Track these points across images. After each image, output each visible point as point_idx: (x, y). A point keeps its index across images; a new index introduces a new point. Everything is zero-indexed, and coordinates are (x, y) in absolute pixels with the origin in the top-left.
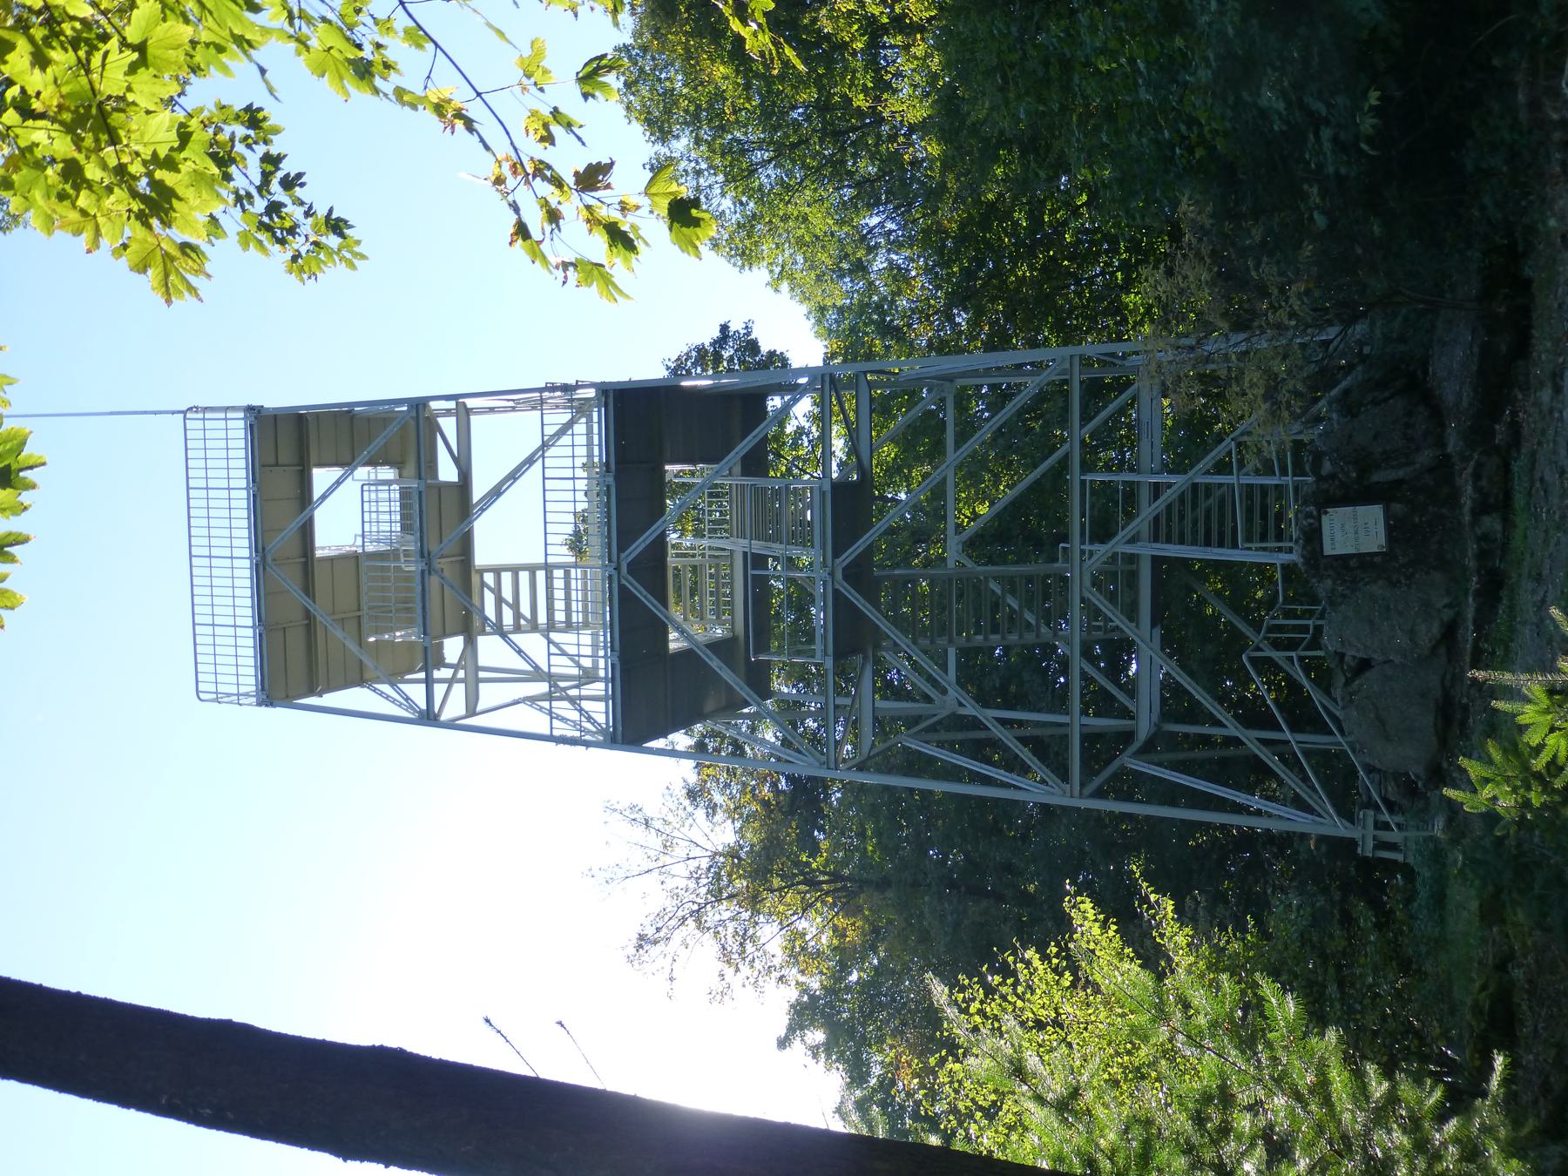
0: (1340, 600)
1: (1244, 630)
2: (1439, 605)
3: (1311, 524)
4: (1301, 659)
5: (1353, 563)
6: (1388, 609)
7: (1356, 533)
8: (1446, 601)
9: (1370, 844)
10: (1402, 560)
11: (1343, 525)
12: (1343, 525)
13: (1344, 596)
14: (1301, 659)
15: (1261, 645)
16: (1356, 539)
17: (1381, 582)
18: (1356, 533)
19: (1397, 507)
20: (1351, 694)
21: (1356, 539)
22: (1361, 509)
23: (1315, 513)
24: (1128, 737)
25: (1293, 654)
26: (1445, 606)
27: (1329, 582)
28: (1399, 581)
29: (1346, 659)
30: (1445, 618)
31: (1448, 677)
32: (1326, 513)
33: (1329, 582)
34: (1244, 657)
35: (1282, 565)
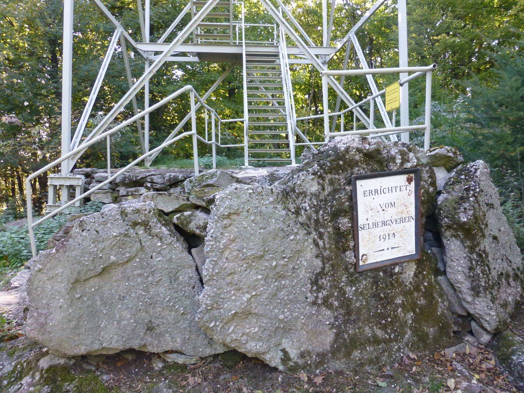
0: (292, 207)
1: (176, 129)
2: (286, 344)
3: (393, 159)
4: (191, 137)
5: (344, 222)
6: (281, 277)
7: (384, 223)
8: (293, 354)
9: (57, 183)
10: (350, 291)
11: (393, 205)
12: (393, 205)
13: (297, 213)
14: (191, 137)
15: (199, 103)
16: (375, 225)
17: (318, 263)
18: (384, 223)
19: (410, 271)
20: (145, 225)
21: (375, 225)
22: (411, 227)
23: (408, 165)
24: (137, 33)
25: (194, 131)
26: (284, 351)
27: (314, 188)
28: (320, 288)
29: (200, 215)
30: (267, 358)
31: (181, 360)
32: (409, 180)
33: (314, 188)
34: (189, 87)
35: (323, 118)
